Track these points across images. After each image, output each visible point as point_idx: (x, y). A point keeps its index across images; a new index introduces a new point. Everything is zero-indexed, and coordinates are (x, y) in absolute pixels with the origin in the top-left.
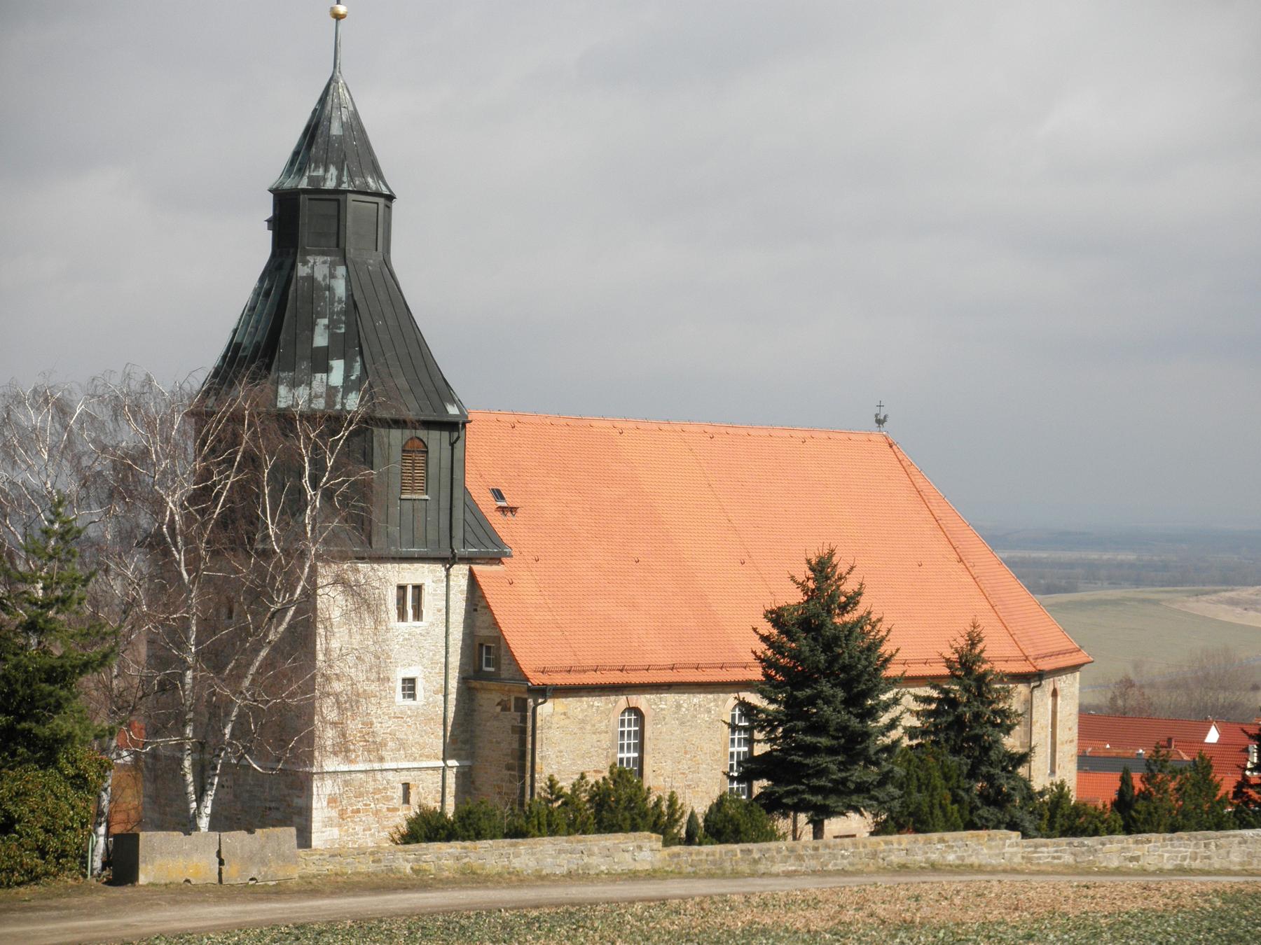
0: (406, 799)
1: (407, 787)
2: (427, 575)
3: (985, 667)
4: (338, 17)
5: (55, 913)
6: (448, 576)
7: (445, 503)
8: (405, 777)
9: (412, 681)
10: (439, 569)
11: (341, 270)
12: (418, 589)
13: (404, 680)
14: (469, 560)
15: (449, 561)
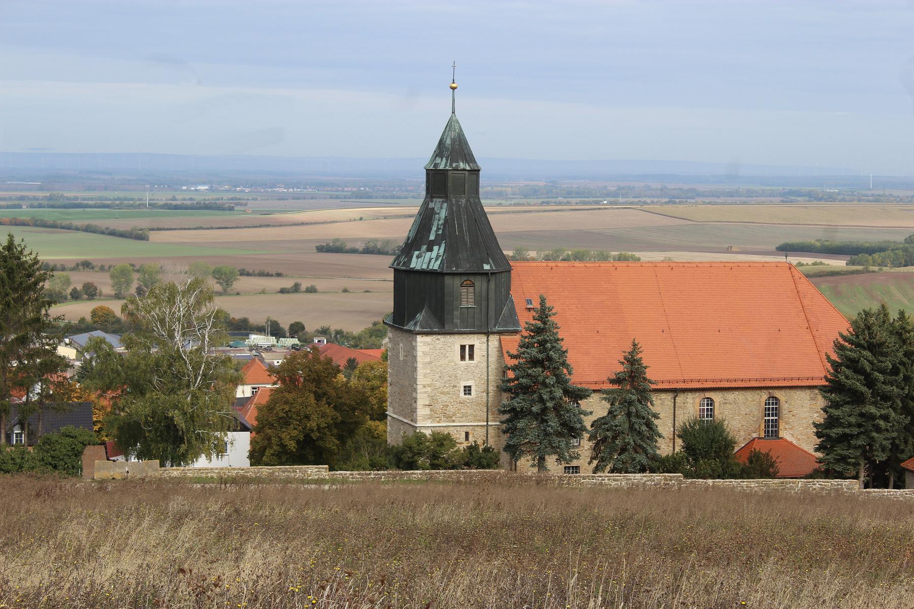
0: (467, 438)
1: (467, 434)
2: (478, 341)
3: (145, 524)
4: (453, 89)
5: (896, 193)
6: (488, 341)
7: (484, 310)
8: (465, 429)
9: (470, 387)
10: (483, 338)
11: (445, 205)
12: (472, 347)
13: (465, 387)
14: (500, 333)
15: (488, 334)
